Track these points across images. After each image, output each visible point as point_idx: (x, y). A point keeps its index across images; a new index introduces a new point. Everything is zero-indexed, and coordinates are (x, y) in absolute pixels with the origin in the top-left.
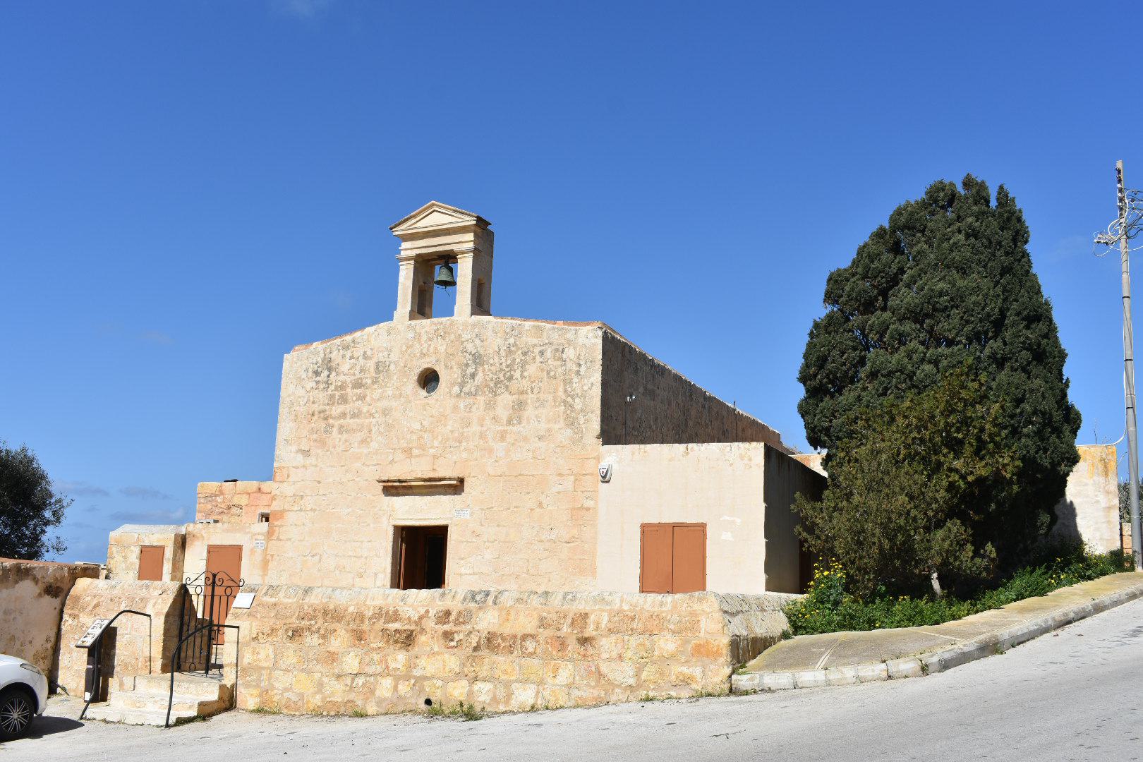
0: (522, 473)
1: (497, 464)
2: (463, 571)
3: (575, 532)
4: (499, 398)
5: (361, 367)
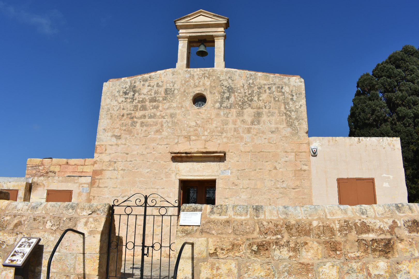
0: (262, 151)
1: (246, 145)
3: (298, 183)
4: (245, 111)
5: (155, 91)
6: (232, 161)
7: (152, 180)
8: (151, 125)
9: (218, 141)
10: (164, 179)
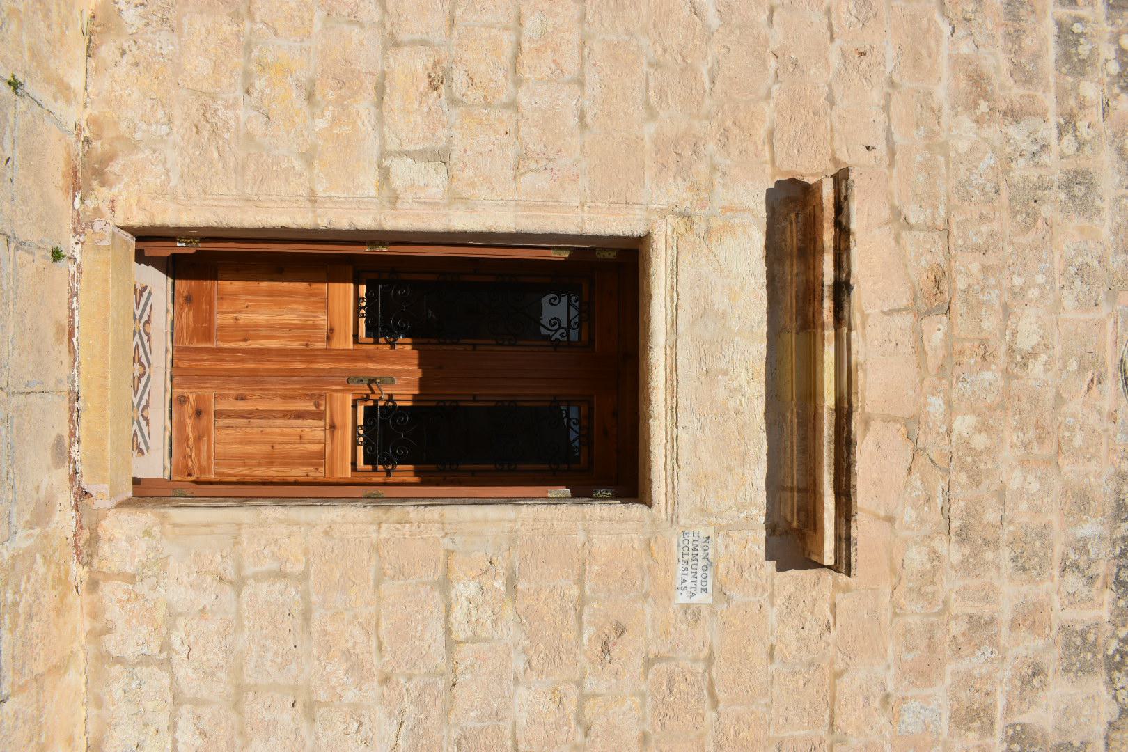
1: (876, 703)
2: (464, 589)
4: (1097, 685)
6: (773, 615)
7: (644, 41)
8: (1015, 37)
9: (914, 506)
10: (650, 129)
